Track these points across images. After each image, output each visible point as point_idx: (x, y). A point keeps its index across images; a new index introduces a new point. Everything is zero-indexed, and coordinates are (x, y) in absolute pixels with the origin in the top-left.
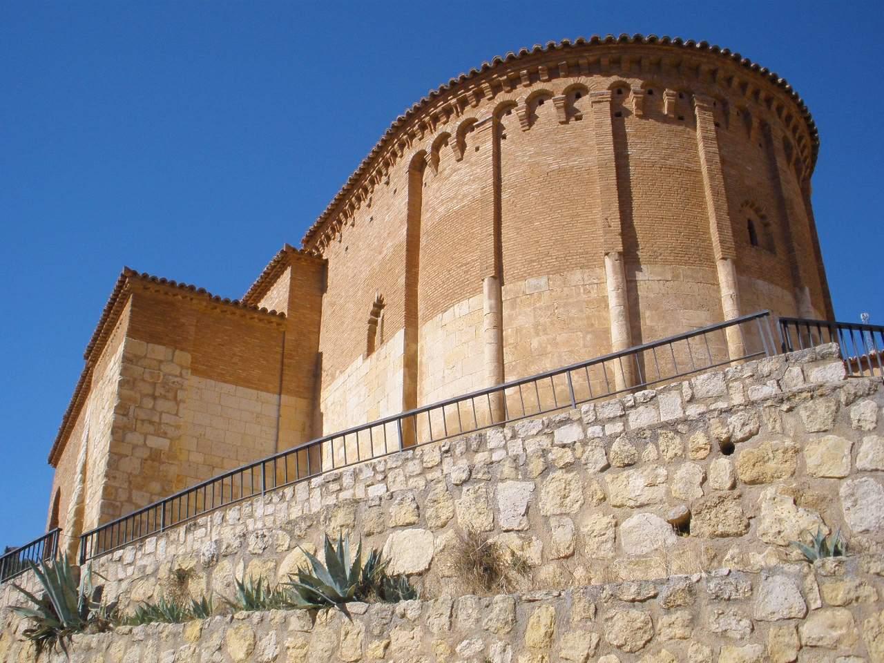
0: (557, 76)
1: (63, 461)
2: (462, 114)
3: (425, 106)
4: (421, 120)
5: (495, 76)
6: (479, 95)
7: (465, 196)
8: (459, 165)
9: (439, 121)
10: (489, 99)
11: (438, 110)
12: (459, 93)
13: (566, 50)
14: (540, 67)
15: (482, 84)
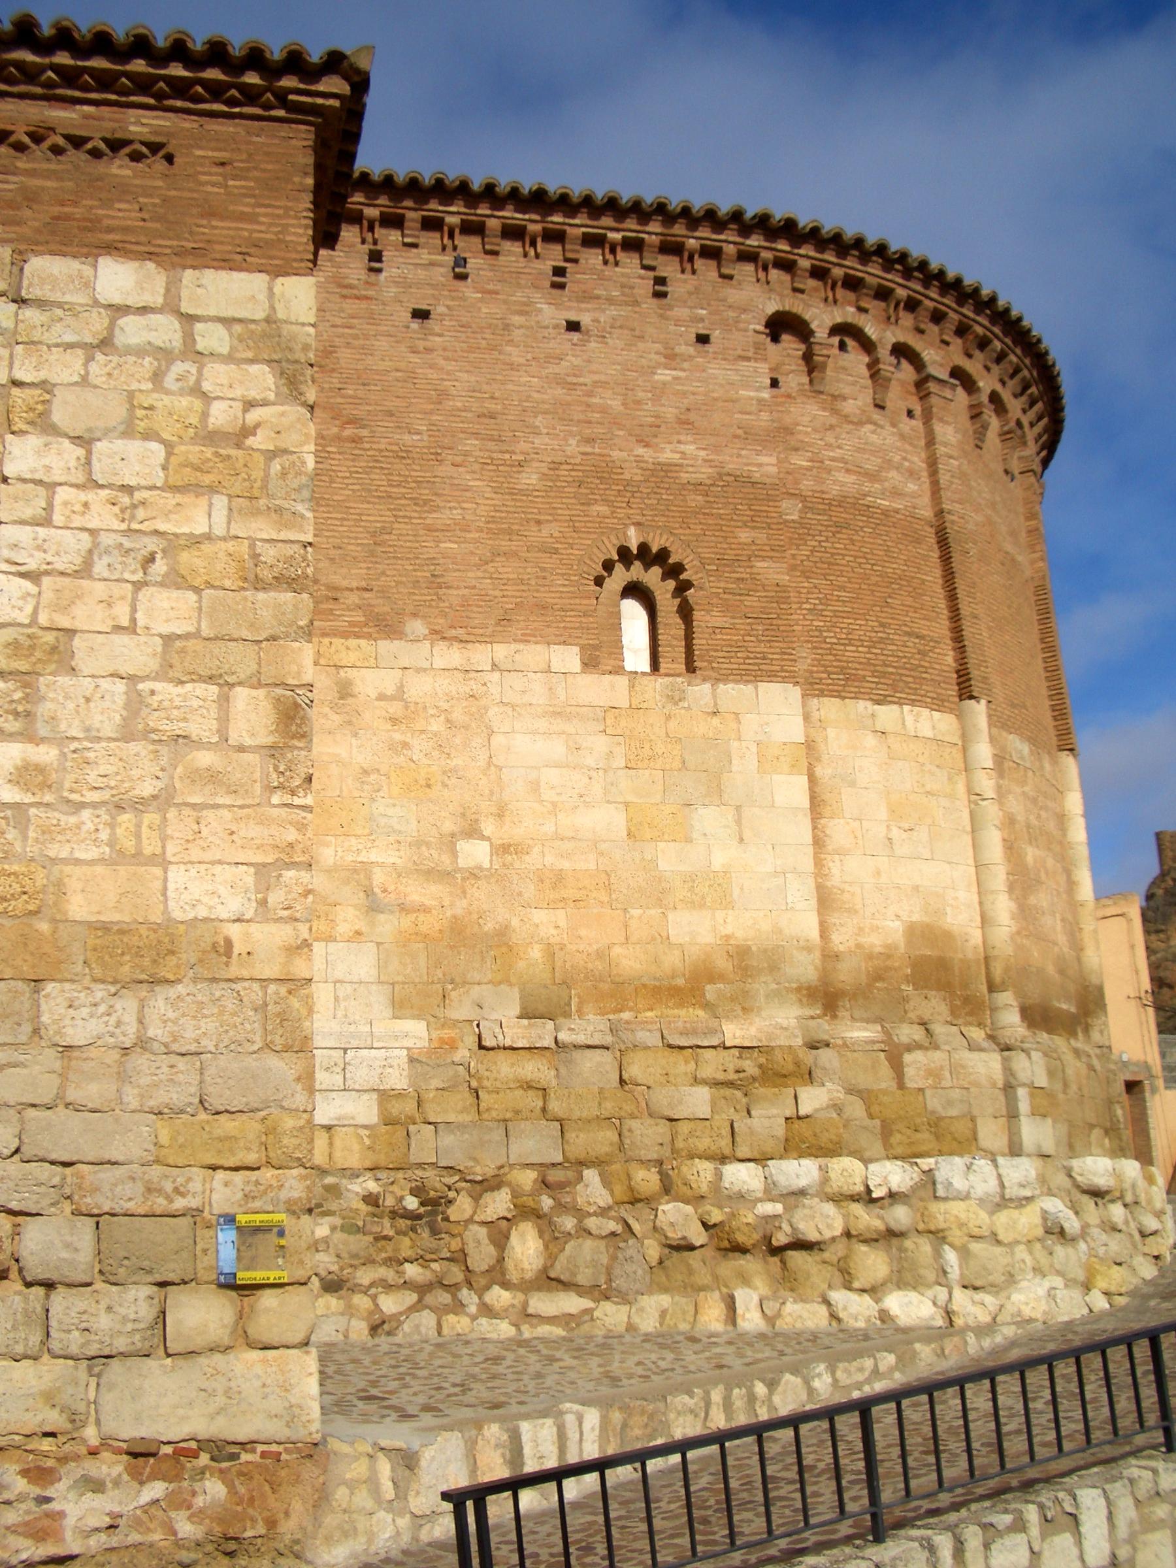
7: (896, 493)
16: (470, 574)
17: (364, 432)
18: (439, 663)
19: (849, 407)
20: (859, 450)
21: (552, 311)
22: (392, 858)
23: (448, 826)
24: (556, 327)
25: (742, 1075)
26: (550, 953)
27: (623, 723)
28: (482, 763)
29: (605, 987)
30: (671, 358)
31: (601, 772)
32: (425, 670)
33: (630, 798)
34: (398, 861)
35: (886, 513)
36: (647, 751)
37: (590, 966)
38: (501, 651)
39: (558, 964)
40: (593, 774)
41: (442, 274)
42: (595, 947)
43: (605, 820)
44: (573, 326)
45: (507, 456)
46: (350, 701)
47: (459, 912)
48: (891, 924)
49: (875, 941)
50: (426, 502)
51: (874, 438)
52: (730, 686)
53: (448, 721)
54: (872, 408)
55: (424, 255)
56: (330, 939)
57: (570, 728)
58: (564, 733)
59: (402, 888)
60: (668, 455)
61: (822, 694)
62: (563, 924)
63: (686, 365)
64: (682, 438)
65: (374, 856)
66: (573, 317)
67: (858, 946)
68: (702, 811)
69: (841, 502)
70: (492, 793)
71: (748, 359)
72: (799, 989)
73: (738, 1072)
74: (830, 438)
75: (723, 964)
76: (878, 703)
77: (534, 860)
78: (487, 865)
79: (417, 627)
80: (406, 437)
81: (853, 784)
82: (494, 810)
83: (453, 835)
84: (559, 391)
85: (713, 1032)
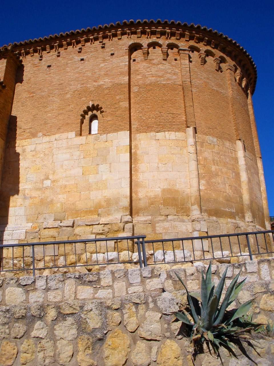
0: (217, 49)
1: (126, 53)
2: (170, 39)
3: (151, 24)
4: (144, 28)
5: (194, 32)
6: (182, 36)
7: (168, 79)
8: (164, 62)
9: (156, 35)
10: (186, 40)
11: (157, 30)
12: (173, 29)
13: (224, 40)
14: (213, 41)
15: (186, 32)
16: (53, 120)
17: (35, 94)
18: (44, 141)
19: (155, 62)
20: (157, 71)
21: (78, 58)
22: (30, 187)
23: (42, 178)
24: (78, 61)
25: (104, 231)
26: (62, 204)
27: (83, 147)
28: (51, 162)
29: (74, 212)
30: (104, 61)
31: (77, 160)
32: (41, 143)
33: (84, 165)
34: (31, 187)
35: (164, 85)
36: (89, 153)
37: (71, 207)
38: (57, 136)
39: (63, 207)
40: (76, 161)
41: (55, 57)
42: (72, 202)
43: (78, 171)
44: (82, 60)
45: (64, 92)
46: (25, 153)
47: (42, 197)
48: (157, 189)
49: (152, 194)
50: (45, 106)
51: (162, 67)
52: (111, 134)
53: (44, 154)
54: (162, 60)
55: (51, 54)
56: (16, 206)
57: (71, 151)
58: (70, 152)
59: (31, 193)
60: (101, 83)
61: (140, 132)
62: (65, 198)
63: (108, 61)
64: (105, 78)
65: (26, 187)
66: (82, 58)
67: (146, 196)
68: (101, 166)
69: (150, 84)
70: (52, 169)
71: (123, 56)
72: (123, 208)
73: (103, 230)
74: (148, 70)
75: (104, 203)
76: (157, 132)
77: (60, 183)
78: (49, 186)
79: (40, 134)
80: (43, 93)
81: (148, 154)
82: (52, 173)
83: (43, 180)
84: (77, 75)
85: (97, 220)
